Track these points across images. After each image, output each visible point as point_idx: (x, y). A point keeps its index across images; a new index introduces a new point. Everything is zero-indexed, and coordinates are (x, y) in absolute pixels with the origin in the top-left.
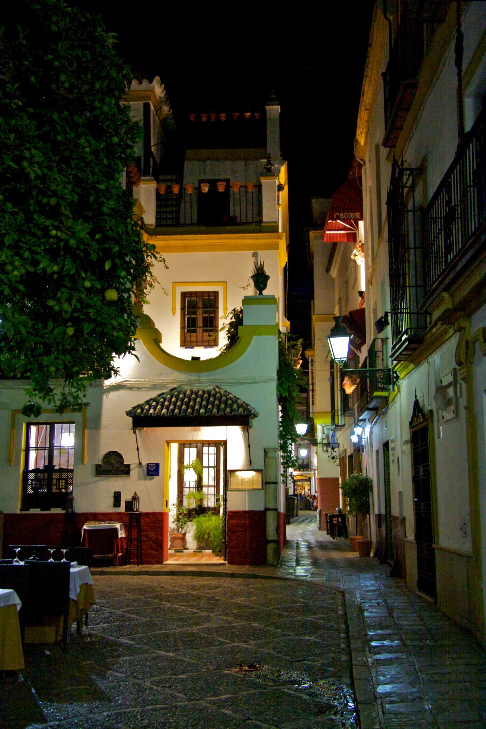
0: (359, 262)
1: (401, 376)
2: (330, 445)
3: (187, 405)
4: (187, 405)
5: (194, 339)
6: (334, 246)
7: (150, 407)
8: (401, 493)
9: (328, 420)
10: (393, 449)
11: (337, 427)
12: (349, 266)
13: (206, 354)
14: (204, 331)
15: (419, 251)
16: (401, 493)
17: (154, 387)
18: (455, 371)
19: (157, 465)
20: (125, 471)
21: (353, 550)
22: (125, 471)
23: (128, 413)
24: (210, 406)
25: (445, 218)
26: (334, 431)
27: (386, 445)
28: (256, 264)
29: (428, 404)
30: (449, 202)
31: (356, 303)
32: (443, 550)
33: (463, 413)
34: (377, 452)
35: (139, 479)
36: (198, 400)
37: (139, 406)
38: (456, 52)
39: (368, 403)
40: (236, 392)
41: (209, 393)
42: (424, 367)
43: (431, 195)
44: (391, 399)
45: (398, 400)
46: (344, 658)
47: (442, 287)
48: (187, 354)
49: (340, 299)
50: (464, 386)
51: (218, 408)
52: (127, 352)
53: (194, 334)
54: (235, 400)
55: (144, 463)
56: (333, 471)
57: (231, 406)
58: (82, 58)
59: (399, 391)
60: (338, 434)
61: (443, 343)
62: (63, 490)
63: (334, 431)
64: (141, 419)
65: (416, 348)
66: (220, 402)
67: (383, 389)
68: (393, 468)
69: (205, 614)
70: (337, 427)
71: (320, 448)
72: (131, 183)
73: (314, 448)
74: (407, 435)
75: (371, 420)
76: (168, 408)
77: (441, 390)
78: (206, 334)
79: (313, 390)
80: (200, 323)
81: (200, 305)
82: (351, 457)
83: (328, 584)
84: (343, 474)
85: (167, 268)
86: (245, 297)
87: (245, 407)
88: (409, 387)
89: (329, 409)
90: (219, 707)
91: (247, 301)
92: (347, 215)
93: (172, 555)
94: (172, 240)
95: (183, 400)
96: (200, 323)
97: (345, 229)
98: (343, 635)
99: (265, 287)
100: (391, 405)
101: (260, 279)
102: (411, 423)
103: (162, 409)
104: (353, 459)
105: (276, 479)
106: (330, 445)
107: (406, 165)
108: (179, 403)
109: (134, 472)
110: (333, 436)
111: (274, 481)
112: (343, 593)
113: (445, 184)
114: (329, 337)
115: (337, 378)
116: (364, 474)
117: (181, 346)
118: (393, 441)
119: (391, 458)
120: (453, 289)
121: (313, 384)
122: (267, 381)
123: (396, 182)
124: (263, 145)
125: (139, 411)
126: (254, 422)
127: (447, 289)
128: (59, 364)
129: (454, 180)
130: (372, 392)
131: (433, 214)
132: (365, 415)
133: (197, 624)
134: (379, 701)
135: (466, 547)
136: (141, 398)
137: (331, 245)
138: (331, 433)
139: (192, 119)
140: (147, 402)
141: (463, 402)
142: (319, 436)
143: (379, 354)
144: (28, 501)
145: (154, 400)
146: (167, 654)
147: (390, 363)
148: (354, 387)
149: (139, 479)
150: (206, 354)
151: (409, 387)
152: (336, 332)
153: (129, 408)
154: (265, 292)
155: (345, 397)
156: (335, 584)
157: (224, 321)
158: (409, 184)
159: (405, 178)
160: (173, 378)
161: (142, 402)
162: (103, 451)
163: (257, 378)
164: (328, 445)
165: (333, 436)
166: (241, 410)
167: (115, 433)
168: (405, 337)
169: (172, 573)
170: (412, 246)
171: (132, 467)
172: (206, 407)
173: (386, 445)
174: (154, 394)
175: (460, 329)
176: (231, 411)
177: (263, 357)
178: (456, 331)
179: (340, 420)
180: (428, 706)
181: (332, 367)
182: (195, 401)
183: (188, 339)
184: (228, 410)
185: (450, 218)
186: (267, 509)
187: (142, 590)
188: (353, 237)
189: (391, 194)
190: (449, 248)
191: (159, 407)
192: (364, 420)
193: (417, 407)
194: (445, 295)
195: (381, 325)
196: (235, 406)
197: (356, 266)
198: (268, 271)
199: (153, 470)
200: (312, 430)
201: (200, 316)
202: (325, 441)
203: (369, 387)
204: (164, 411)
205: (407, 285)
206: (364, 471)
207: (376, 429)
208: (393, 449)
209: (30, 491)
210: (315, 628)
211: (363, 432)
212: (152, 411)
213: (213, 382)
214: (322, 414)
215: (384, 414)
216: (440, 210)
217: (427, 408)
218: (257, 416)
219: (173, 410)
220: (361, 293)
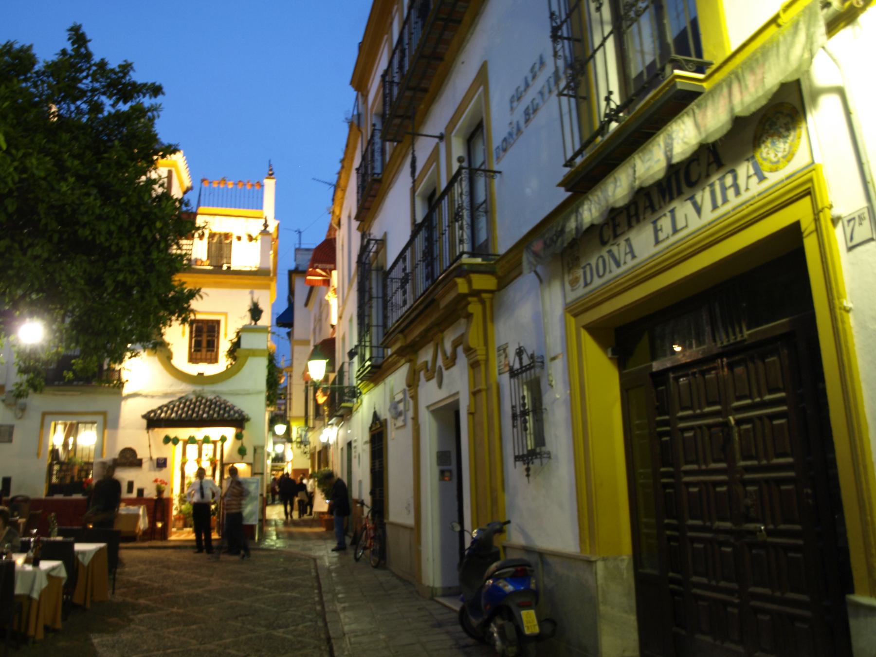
0: (331, 303)
1: (364, 391)
2: (303, 442)
3: (193, 410)
4: (193, 410)
5: (199, 357)
6: (312, 289)
7: (162, 412)
8: (360, 482)
9: (302, 423)
10: (355, 447)
11: (308, 428)
12: (324, 306)
13: (208, 369)
14: (208, 351)
15: (380, 300)
17: (166, 395)
18: (404, 391)
19: (165, 460)
20: (138, 463)
21: (320, 525)
22: (138, 463)
23: (144, 417)
24: (211, 412)
25: (401, 280)
26: (307, 431)
27: (349, 444)
28: (252, 299)
29: (385, 414)
30: (404, 269)
31: (327, 334)
32: (393, 524)
33: (410, 423)
34: (342, 449)
35: (150, 470)
36: (202, 406)
37: (152, 411)
39: (336, 411)
40: (232, 400)
41: (211, 401)
42: (381, 387)
44: (354, 409)
45: (360, 409)
46: (319, 608)
47: (397, 331)
48: (194, 369)
49: (315, 329)
50: (411, 402)
51: (219, 414)
53: (199, 353)
54: (232, 408)
55: (155, 457)
56: (305, 463)
57: (229, 412)
59: (361, 403)
60: (310, 434)
63: (307, 431)
64: (153, 421)
65: (376, 374)
66: (216, 406)
67: (348, 401)
68: (355, 462)
69: (206, 579)
70: (308, 428)
71: (294, 445)
73: (289, 445)
74: (367, 437)
75: (337, 424)
76: (177, 412)
77: (394, 405)
78: (209, 353)
79: (290, 399)
80: (204, 344)
81: (205, 330)
82: (320, 452)
83: (303, 553)
84: (313, 466)
87: (240, 413)
88: (369, 402)
89: (303, 414)
90: (225, 648)
91: (245, 329)
92: (324, 266)
93: (175, 533)
95: (189, 406)
96: (204, 344)
97: (321, 275)
98: (316, 591)
99: (259, 319)
100: (354, 413)
101: (256, 312)
102: (371, 428)
103: (171, 414)
104: (322, 454)
105: (263, 469)
106: (303, 442)
107: (372, 237)
108: (186, 409)
109: (146, 465)
110: (306, 435)
111: (260, 471)
112: (315, 559)
113: (402, 256)
114: (310, 359)
116: (330, 468)
118: (355, 441)
119: (353, 454)
120: (406, 331)
121: (290, 394)
122: (259, 393)
123: (364, 249)
124: (260, 206)
125: (152, 415)
126: (247, 425)
127: (402, 332)
129: (408, 254)
130: (340, 403)
131: (393, 274)
132: (333, 420)
133: (200, 587)
134: (347, 636)
135: (410, 521)
136: (154, 404)
138: (304, 433)
140: (160, 408)
141: (410, 414)
142: (294, 435)
143: (346, 374)
144: (52, 489)
145: (166, 406)
147: (355, 382)
148: (325, 398)
149: (150, 470)
150: (208, 369)
151: (369, 402)
152: (314, 355)
153: (144, 413)
154: (260, 323)
155: (317, 406)
156: (308, 553)
157: (224, 345)
158: (374, 250)
159: (371, 246)
160: (183, 389)
161: (155, 407)
162: (120, 447)
163: (249, 391)
164: (301, 442)
165: (306, 435)
166: (237, 415)
167: (131, 433)
168: (368, 363)
169: (175, 547)
171: (144, 461)
172: (208, 412)
173: (349, 444)
174: (165, 401)
175: (410, 361)
176: (229, 416)
177: (256, 373)
178: (406, 362)
179: (311, 424)
180: (382, 637)
181: (307, 383)
182: (199, 406)
183: (194, 357)
184: (226, 415)
185: (404, 281)
187: (151, 562)
188: (327, 282)
189: (360, 257)
190: (405, 302)
191: (169, 412)
192: (332, 424)
193: (375, 416)
194: (400, 336)
195: (352, 354)
196: (232, 412)
197: (327, 304)
198: (261, 306)
199: (162, 464)
200: (288, 431)
201: (204, 339)
202: (299, 440)
203: (338, 402)
204: (174, 415)
206: (330, 464)
207: (342, 432)
208: (355, 447)
209: (54, 480)
210: (295, 586)
211: (331, 434)
212: (163, 415)
213: (214, 392)
214: (297, 418)
215: (349, 420)
216: (397, 273)
217: (383, 417)
219: (181, 414)
220: (333, 326)
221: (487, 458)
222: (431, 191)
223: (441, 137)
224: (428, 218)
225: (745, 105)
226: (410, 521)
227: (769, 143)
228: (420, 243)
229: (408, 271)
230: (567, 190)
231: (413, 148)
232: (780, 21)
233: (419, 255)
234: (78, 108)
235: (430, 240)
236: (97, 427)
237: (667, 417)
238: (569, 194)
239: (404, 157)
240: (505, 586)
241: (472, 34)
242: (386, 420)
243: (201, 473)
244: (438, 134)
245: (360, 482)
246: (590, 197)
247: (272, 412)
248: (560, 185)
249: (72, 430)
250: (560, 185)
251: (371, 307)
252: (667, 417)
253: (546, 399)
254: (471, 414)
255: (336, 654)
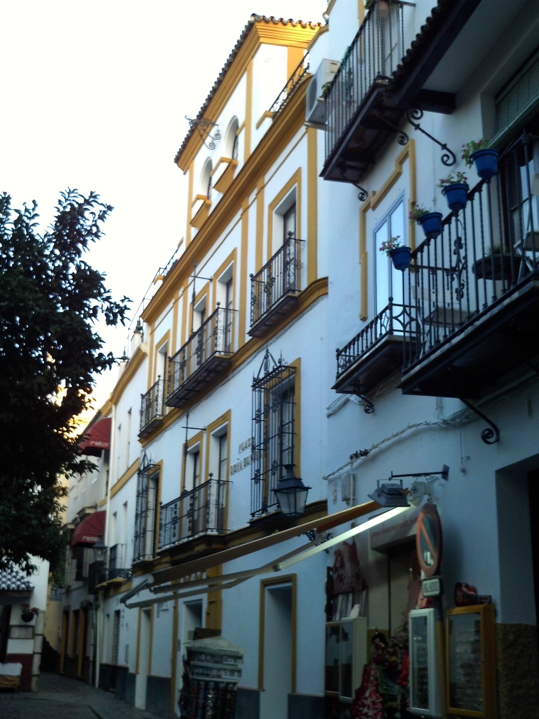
16: (127, 646)
30: (184, 357)
38: (179, 642)
43: (192, 239)
52: (102, 282)
58: (118, 312)
61: (301, 312)
62: (400, 681)
72: (53, 242)
82: (76, 612)
85: (34, 202)
86: (97, 271)
94: (87, 557)
115: (223, 497)
117: (261, 580)
122: (86, 422)
128: (23, 578)
137: (67, 492)
139: (6, 328)
146: (502, 267)
170: (262, 422)
186: (34, 653)
205: (291, 435)
216: (178, 359)
218: (9, 198)
221: (503, 390)
222: (405, 153)
223: (211, 280)
224: (201, 329)
225: (185, 414)
226: (411, 273)
227: (431, 212)
228: (195, 343)
229: (186, 359)
230: (250, 336)
231: (218, 509)
232: (390, 476)
233: (193, 350)
234: (66, 235)
235: (201, 343)
236: (55, 484)
237: (97, 685)
238: (251, 337)
239: (258, 351)
240: (185, 580)
241: (150, 445)
242: (257, 384)
243: (379, 72)
244: (210, 278)
245: (127, 646)
246: (53, 402)
247: (387, 252)
248: (333, 388)
249: (12, 251)
250: (333, 388)
251: (346, 76)
252: (97, 685)
253: (284, 441)
254: (208, 614)
255: (3, 696)
